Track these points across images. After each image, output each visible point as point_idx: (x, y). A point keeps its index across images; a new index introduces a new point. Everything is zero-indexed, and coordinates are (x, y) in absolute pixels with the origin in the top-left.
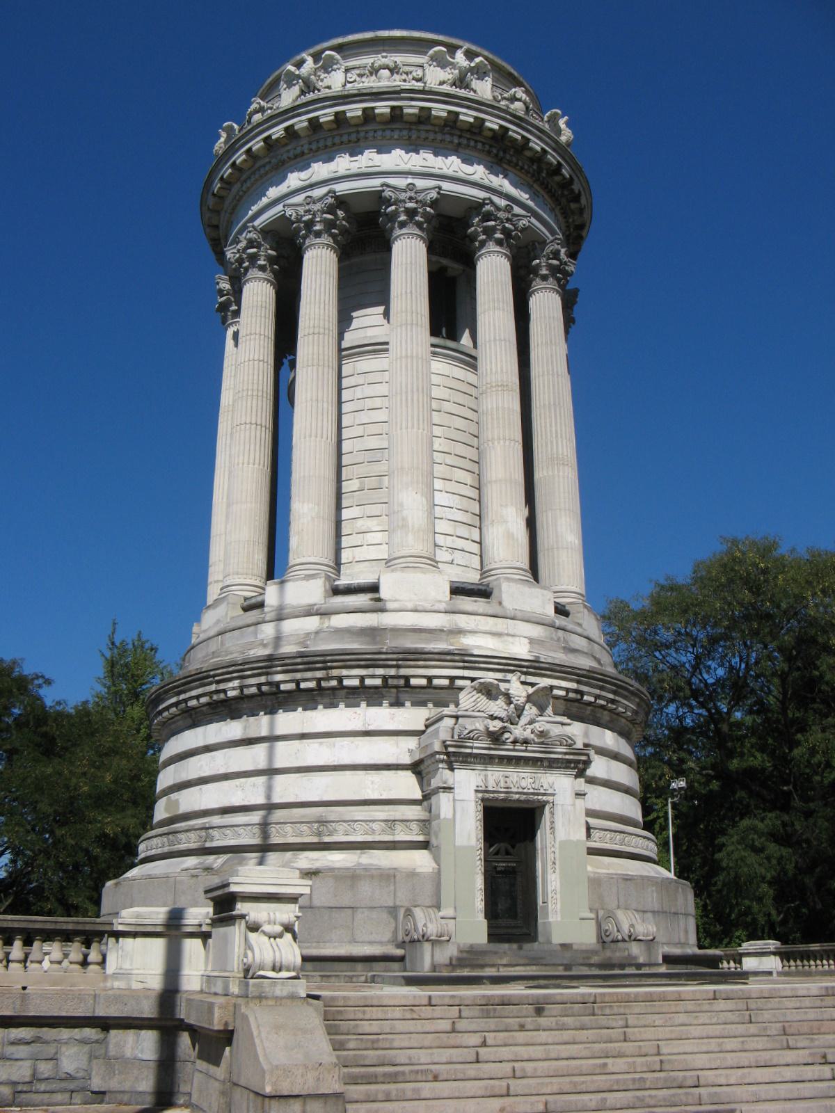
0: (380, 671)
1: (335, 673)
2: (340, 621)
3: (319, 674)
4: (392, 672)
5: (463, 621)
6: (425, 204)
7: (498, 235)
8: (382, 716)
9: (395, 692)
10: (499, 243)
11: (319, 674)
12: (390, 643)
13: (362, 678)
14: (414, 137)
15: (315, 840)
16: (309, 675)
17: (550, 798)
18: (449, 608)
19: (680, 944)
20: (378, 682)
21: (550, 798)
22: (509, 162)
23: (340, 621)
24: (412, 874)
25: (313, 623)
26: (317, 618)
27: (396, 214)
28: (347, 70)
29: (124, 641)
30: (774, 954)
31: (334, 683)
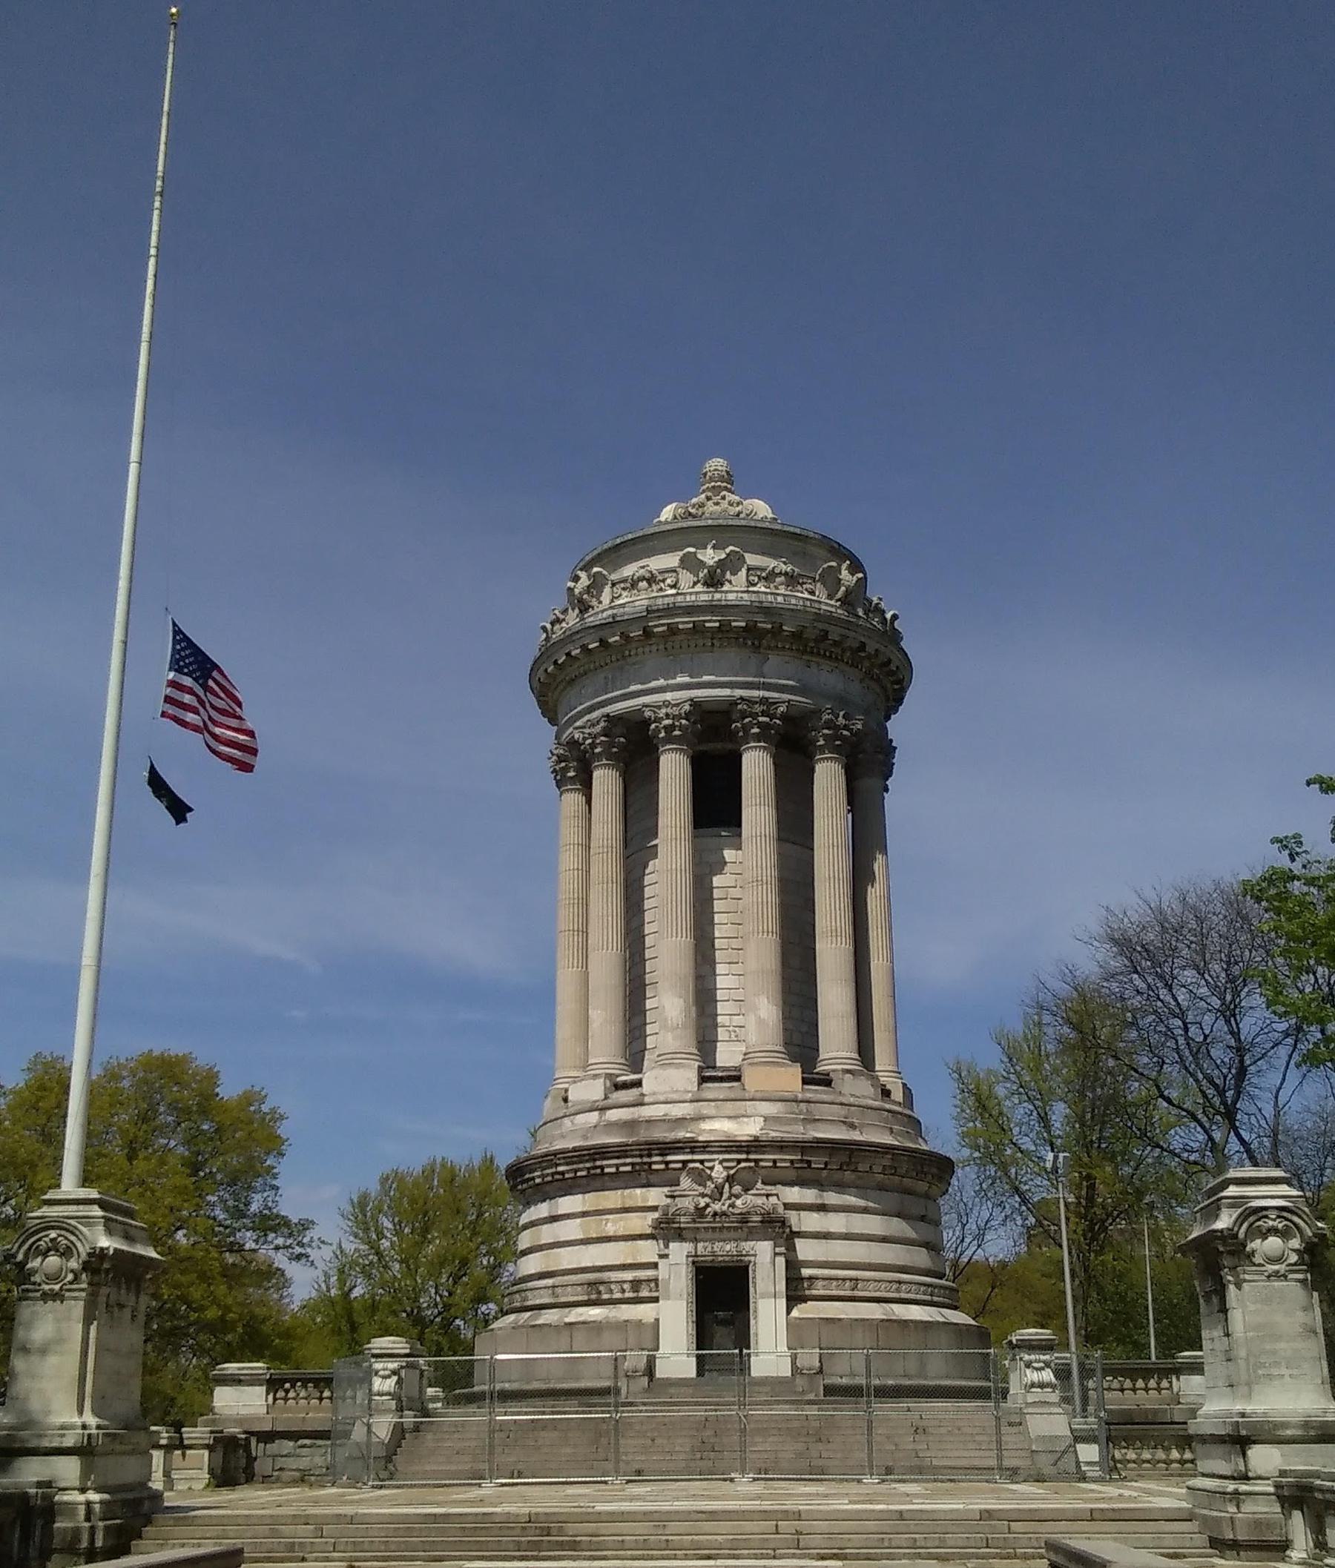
0: (629, 1160)
1: (598, 1163)
2: (613, 1115)
3: (588, 1165)
4: (638, 1160)
5: (707, 1109)
6: (680, 717)
7: (756, 730)
8: (639, 1195)
9: (642, 1176)
10: (758, 738)
11: (588, 1165)
12: (644, 1135)
13: (617, 1166)
14: (669, 648)
15: (586, 1298)
16: (581, 1166)
17: (752, 1259)
18: (696, 1097)
19: (853, 1375)
20: (629, 1168)
21: (752, 1259)
22: (769, 648)
23: (613, 1115)
24: (639, 1323)
25: (593, 1117)
26: (596, 1113)
27: (657, 730)
28: (613, 585)
29: (313, 1223)
30: (1244, 1455)
31: (598, 1171)
